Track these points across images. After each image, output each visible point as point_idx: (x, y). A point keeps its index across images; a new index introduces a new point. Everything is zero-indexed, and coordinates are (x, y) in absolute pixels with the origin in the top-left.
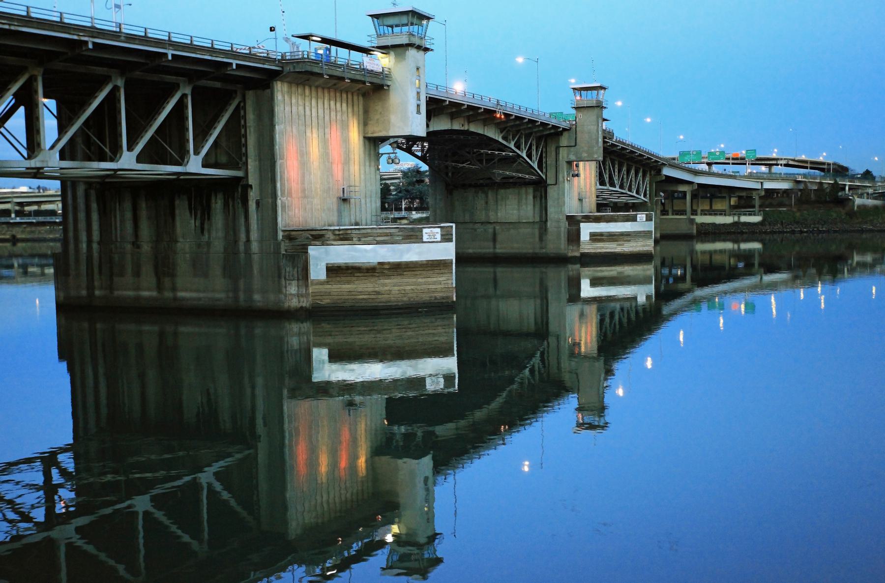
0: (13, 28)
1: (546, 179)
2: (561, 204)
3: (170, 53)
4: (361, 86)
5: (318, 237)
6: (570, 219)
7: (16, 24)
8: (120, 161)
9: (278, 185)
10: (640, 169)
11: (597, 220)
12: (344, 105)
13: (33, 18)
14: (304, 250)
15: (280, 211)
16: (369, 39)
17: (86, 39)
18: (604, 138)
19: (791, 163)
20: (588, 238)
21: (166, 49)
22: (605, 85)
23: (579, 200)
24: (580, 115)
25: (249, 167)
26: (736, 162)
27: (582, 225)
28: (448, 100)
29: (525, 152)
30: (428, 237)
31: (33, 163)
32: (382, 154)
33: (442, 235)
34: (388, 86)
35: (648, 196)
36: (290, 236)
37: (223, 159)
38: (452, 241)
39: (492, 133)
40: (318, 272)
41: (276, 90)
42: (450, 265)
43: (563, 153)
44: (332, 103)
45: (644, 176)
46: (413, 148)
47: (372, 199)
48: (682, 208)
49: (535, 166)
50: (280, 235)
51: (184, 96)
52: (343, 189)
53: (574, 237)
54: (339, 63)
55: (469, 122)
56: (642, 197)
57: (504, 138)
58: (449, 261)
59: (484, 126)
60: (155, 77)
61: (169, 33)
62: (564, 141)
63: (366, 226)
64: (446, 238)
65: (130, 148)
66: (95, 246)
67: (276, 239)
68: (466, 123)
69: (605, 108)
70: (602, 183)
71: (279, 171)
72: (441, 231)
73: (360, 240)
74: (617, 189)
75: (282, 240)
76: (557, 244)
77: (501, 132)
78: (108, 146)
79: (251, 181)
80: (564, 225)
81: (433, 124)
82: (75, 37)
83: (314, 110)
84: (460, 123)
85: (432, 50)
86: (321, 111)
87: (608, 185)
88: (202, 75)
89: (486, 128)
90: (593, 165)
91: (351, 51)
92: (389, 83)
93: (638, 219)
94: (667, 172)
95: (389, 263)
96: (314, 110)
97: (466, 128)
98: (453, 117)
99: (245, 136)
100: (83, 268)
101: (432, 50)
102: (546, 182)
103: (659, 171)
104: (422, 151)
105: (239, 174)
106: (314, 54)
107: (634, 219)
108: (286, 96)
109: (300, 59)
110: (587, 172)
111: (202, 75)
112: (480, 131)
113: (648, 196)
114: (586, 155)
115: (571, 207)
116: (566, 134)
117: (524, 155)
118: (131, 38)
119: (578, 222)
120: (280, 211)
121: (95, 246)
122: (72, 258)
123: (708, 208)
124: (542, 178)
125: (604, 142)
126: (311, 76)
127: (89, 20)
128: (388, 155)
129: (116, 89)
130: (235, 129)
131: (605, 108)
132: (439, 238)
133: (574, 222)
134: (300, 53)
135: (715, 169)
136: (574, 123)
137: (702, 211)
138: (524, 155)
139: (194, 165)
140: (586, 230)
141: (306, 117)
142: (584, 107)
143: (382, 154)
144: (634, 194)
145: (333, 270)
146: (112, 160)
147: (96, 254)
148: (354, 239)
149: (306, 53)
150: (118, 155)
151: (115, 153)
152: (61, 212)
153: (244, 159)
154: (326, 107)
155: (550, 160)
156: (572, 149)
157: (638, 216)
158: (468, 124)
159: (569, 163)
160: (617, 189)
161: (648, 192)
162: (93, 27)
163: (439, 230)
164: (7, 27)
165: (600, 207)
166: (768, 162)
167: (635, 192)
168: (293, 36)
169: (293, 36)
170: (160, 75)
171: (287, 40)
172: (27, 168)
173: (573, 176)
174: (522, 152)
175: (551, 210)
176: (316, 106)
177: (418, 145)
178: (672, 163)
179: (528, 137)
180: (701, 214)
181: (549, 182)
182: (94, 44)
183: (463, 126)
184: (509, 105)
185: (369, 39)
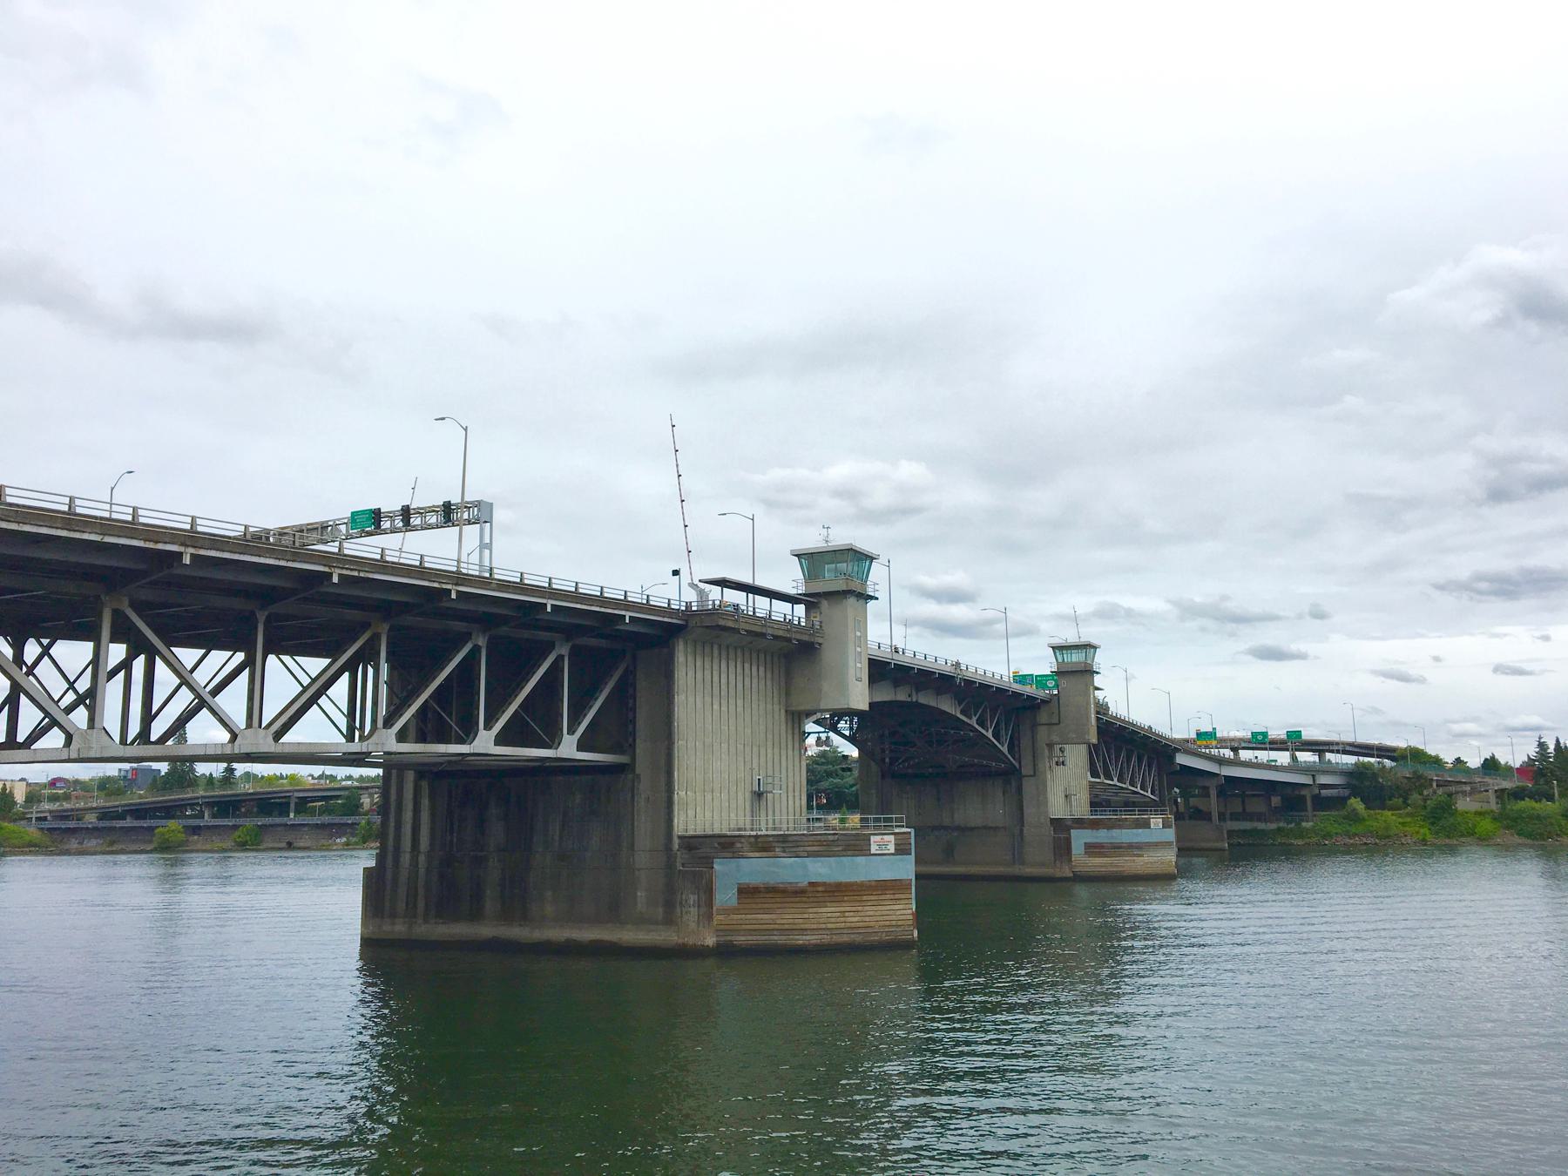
0: (362, 575)
1: (1020, 767)
2: (1041, 800)
3: (628, 614)
4: (785, 644)
5: (727, 845)
6: (1057, 823)
7: (367, 569)
8: (475, 742)
10: (1144, 755)
11: (1094, 825)
12: (762, 669)
13: (388, 562)
14: (902, 847)
16: (795, 584)
17: (449, 587)
18: (1098, 713)
19: (1348, 748)
20: (1082, 850)
21: (545, 598)
22: (1094, 641)
23: (1066, 796)
24: (1064, 682)
25: (638, 751)
26: (1275, 746)
27: (1073, 832)
28: (893, 662)
29: (990, 731)
30: (877, 848)
31: (356, 747)
32: (809, 734)
34: (820, 644)
35: (1157, 792)
36: (692, 843)
38: (910, 854)
39: (948, 706)
40: (725, 896)
43: (1042, 733)
44: (747, 666)
45: (1150, 766)
46: (839, 726)
49: (1005, 749)
50: (676, 842)
51: (560, 658)
52: (759, 779)
53: (1063, 849)
55: (918, 690)
56: (1149, 794)
57: (962, 712)
58: (908, 882)
59: (937, 695)
60: (526, 634)
61: (382, 549)
62: (1043, 717)
64: (901, 850)
65: (488, 727)
66: (422, 858)
67: (671, 850)
68: (914, 693)
69: (1097, 673)
70: (1094, 774)
71: (676, 755)
72: (895, 839)
73: (784, 852)
74: (1115, 782)
75: (678, 850)
76: (1037, 860)
77: (960, 704)
78: (454, 719)
80: (1049, 831)
82: (436, 585)
83: (724, 676)
85: (877, 599)
87: (1102, 776)
89: (939, 697)
90: (1083, 749)
91: (724, 589)
92: (820, 641)
94: (1182, 759)
95: (824, 884)
96: (724, 676)
98: (897, 684)
99: (634, 709)
100: (402, 891)
101: (877, 599)
102: (1019, 771)
103: (1172, 758)
104: (851, 729)
106: (477, 568)
107: (1146, 825)
109: (710, 610)
110: (1076, 757)
111: (405, 608)
112: (933, 703)
113: (1157, 792)
115: (1057, 808)
116: (1044, 709)
117: (990, 735)
118: (505, 585)
119: (1068, 829)
121: (422, 858)
122: (389, 875)
123: (1240, 810)
124: (1015, 766)
125: (1098, 719)
126: (721, 632)
127: (107, 507)
128: (817, 735)
129: (476, 650)
130: (623, 699)
131: (1097, 673)
132: (891, 849)
133: (1061, 826)
134: (710, 603)
135: (1245, 755)
136: (1056, 692)
137: (1231, 814)
138: (990, 735)
139: (568, 748)
140: (1079, 838)
142: (1067, 672)
143: (809, 734)
144: (1139, 790)
145: (747, 892)
146: (461, 741)
147: (422, 871)
148: (777, 850)
150: (472, 735)
151: (467, 732)
153: (631, 740)
155: (1025, 742)
156: (1055, 727)
158: (917, 694)
159: (1050, 746)
160: (1115, 782)
161: (1157, 788)
162: (458, 572)
163: (892, 838)
164: (356, 574)
165: (1095, 804)
166: (1317, 748)
167: (1139, 786)
168: (700, 581)
169: (700, 581)
170: (533, 632)
171: (692, 585)
172: (344, 754)
173: (1057, 764)
174: (987, 731)
175: (1029, 810)
176: (685, 663)
177: (846, 721)
178: (1184, 746)
179: (994, 711)
180: (1231, 820)
181: (1024, 772)
182: (458, 592)
184: (972, 669)
185: (795, 584)
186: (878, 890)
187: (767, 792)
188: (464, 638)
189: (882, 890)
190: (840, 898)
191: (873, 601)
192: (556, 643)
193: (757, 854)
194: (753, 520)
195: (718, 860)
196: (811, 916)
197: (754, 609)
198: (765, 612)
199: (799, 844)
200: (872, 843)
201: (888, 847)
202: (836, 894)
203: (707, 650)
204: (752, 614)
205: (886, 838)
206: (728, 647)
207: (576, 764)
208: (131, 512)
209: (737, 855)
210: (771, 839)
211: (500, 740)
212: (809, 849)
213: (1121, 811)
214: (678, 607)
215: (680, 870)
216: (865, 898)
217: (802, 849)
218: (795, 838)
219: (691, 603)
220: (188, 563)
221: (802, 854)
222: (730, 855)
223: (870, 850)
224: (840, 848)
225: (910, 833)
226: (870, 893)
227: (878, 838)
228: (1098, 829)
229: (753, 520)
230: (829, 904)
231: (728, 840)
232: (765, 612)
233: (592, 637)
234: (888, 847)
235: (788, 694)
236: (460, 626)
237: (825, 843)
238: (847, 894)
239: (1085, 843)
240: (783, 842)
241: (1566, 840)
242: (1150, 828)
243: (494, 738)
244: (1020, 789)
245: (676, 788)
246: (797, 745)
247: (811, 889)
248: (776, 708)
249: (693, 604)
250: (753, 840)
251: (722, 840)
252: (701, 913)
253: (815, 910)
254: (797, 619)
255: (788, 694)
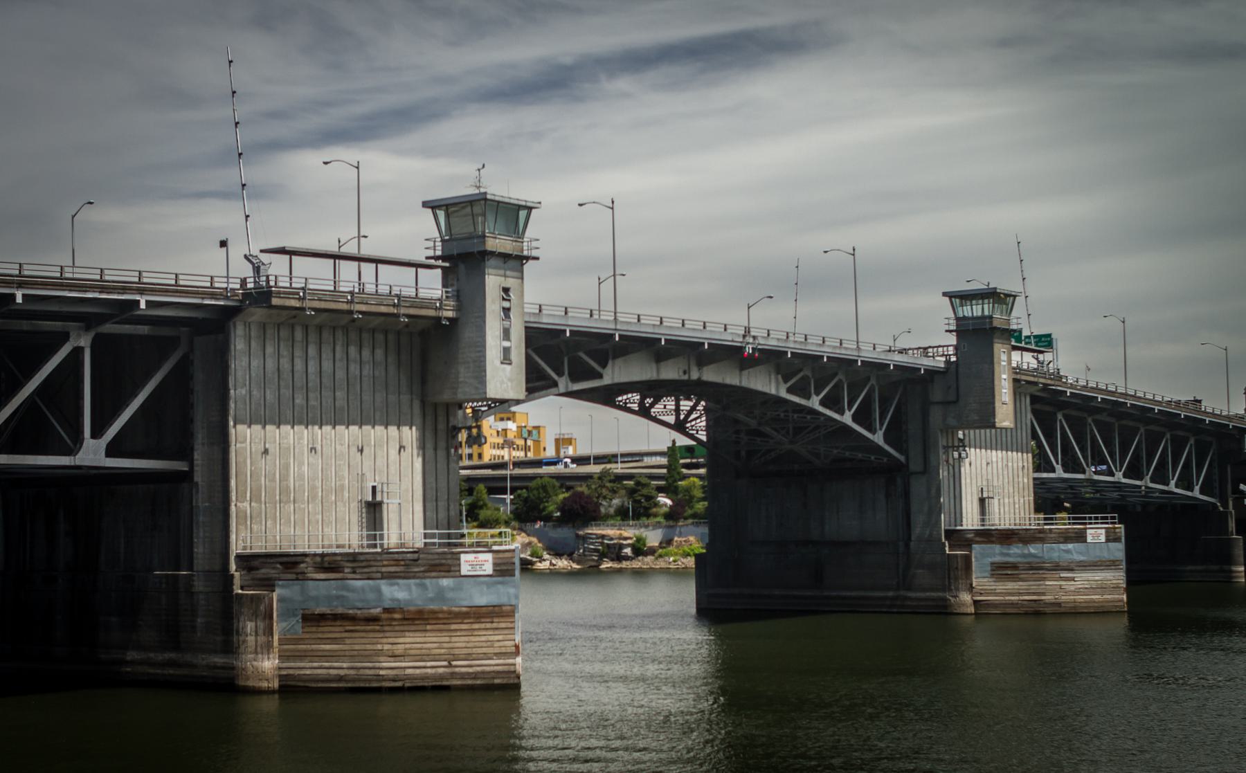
9: (233, 483)
12: (379, 353)
15: (234, 524)
16: (947, 321)
30: (470, 568)
33: (495, 564)
37: (480, 412)
41: (232, 335)
42: (512, 614)
44: (353, 350)
47: (439, 503)
48: (377, 529)
54: (341, 289)
63: (401, 548)
64: (1111, 538)
65: (97, 433)
72: (494, 558)
73: (354, 572)
79: (198, 477)
81: (613, 366)
84: (679, 369)
85: (537, 258)
86: (327, 366)
88: (101, 319)
89: (745, 372)
91: (1023, 352)
93: (1089, 539)
95: (402, 610)
97: (695, 375)
105: (180, 466)
108: (253, 344)
111: (101, 319)
114: (976, 418)
120: (234, 524)
132: (489, 569)
141: (296, 375)
149: (272, 278)
150: (78, 446)
152: (558, 514)
154: (338, 355)
157: (1089, 531)
163: (489, 557)
168: (262, 251)
169: (262, 251)
170: (33, 322)
183: (685, 373)
186: (469, 618)
187: (989, 498)
188: (65, 337)
189: (474, 617)
190: (420, 627)
191: (531, 262)
192: (71, 334)
193: (322, 576)
194: (358, 168)
195: (280, 583)
196: (386, 647)
197: (615, 313)
198: (352, 284)
199: (392, 563)
200: (1088, 535)
201: (484, 568)
202: (417, 622)
203: (284, 333)
204: (1026, 367)
205: (482, 557)
206: (1020, 394)
207: (101, 471)
208: (174, 277)
209: (301, 577)
210: (339, 558)
211: (112, 451)
212: (384, 569)
213: (1090, 518)
214: (225, 285)
215: (237, 594)
216: (453, 627)
217: (374, 569)
218: (368, 557)
219: (245, 279)
220: (21, 302)
221: (374, 575)
222: (294, 576)
223: (459, 571)
224: (422, 569)
225: (1120, 528)
226: (460, 621)
227: (470, 557)
228: (1010, 544)
229: (358, 168)
230: (407, 634)
231: (293, 559)
232: (352, 284)
233: (114, 323)
234: (484, 568)
235: (424, 382)
236: (57, 325)
237: (402, 563)
238: (431, 622)
239: (992, 564)
240: (354, 561)
241: (1238, 642)
242: (1086, 541)
243: (105, 446)
244: (907, 494)
245: (234, 498)
246: (442, 444)
247: (385, 616)
248: (405, 398)
249: (248, 280)
250: (318, 559)
251: (285, 559)
252: (259, 643)
253: (391, 640)
254: (1026, 364)
255: (424, 382)
